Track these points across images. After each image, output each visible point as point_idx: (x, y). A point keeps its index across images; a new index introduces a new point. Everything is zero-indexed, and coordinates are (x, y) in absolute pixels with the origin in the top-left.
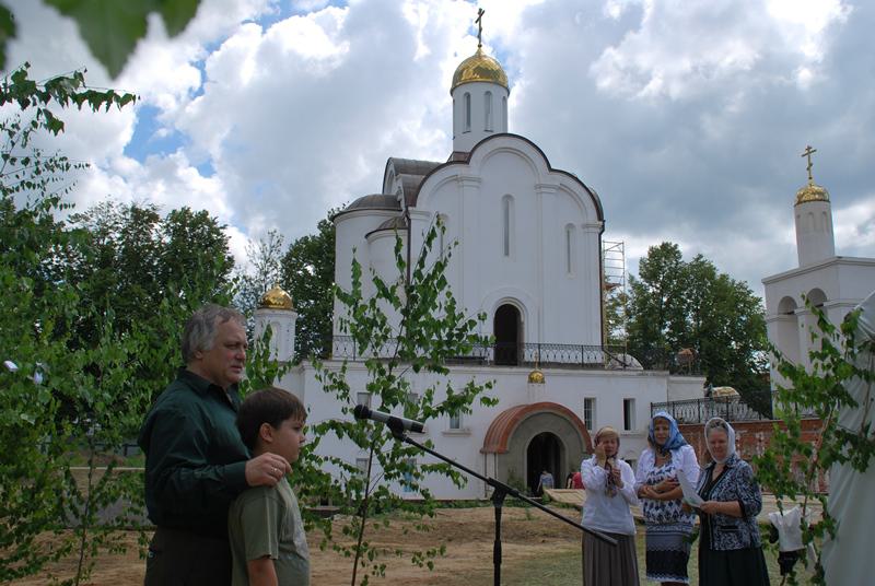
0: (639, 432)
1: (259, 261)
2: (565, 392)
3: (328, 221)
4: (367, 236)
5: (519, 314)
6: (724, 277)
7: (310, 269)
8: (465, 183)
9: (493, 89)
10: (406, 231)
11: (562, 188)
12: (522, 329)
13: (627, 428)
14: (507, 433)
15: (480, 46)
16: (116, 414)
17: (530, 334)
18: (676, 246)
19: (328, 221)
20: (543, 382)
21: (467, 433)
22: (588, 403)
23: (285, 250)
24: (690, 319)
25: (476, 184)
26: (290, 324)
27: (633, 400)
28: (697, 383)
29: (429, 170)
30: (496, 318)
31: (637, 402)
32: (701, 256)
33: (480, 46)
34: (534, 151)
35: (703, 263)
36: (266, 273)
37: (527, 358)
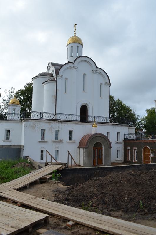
0: (121, 142)
1: (8, 95)
2: (102, 130)
3: (27, 86)
4: (43, 84)
5: (87, 107)
6: (124, 104)
7: (22, 98)
8: (73, 69)
9: (80, 46)
10: (56, 82)
11: (100, 73)
12: (88, 112)
13: (118, 141)
14: (88, 142)
15: (75, 34)
16: (143, 190)
17: (90, 113)
18: (113, 96)
19: (27, 86)
20: (97, 127)
21: (74, 142)
22: (108, 133)
23: (16, 92)
24: (116, 114)
25: (76, 69)
26: (19, 109)
27: (119, 133)
28: (134, 128)
29: (62, 66)
30: (81, 109)
31: (110, 133)
32: (119, 99)
33: (75, 34)
34: (92, 62)
35: (119, 101)
36: (10, 98)
37: (89, 120)
